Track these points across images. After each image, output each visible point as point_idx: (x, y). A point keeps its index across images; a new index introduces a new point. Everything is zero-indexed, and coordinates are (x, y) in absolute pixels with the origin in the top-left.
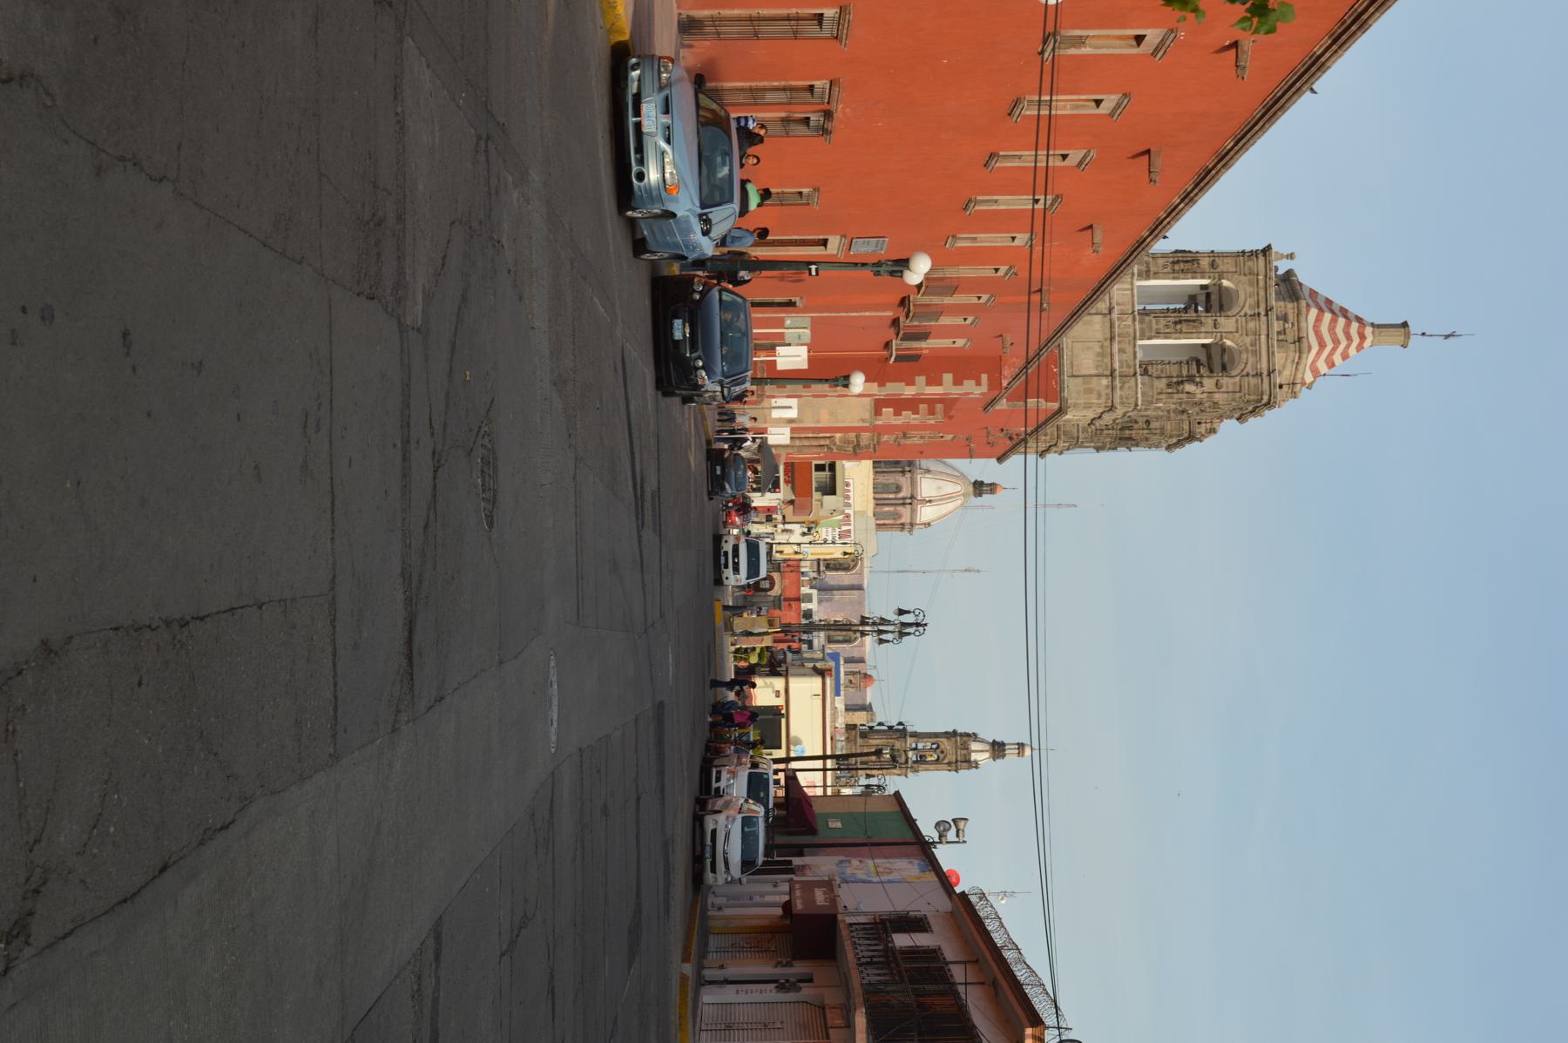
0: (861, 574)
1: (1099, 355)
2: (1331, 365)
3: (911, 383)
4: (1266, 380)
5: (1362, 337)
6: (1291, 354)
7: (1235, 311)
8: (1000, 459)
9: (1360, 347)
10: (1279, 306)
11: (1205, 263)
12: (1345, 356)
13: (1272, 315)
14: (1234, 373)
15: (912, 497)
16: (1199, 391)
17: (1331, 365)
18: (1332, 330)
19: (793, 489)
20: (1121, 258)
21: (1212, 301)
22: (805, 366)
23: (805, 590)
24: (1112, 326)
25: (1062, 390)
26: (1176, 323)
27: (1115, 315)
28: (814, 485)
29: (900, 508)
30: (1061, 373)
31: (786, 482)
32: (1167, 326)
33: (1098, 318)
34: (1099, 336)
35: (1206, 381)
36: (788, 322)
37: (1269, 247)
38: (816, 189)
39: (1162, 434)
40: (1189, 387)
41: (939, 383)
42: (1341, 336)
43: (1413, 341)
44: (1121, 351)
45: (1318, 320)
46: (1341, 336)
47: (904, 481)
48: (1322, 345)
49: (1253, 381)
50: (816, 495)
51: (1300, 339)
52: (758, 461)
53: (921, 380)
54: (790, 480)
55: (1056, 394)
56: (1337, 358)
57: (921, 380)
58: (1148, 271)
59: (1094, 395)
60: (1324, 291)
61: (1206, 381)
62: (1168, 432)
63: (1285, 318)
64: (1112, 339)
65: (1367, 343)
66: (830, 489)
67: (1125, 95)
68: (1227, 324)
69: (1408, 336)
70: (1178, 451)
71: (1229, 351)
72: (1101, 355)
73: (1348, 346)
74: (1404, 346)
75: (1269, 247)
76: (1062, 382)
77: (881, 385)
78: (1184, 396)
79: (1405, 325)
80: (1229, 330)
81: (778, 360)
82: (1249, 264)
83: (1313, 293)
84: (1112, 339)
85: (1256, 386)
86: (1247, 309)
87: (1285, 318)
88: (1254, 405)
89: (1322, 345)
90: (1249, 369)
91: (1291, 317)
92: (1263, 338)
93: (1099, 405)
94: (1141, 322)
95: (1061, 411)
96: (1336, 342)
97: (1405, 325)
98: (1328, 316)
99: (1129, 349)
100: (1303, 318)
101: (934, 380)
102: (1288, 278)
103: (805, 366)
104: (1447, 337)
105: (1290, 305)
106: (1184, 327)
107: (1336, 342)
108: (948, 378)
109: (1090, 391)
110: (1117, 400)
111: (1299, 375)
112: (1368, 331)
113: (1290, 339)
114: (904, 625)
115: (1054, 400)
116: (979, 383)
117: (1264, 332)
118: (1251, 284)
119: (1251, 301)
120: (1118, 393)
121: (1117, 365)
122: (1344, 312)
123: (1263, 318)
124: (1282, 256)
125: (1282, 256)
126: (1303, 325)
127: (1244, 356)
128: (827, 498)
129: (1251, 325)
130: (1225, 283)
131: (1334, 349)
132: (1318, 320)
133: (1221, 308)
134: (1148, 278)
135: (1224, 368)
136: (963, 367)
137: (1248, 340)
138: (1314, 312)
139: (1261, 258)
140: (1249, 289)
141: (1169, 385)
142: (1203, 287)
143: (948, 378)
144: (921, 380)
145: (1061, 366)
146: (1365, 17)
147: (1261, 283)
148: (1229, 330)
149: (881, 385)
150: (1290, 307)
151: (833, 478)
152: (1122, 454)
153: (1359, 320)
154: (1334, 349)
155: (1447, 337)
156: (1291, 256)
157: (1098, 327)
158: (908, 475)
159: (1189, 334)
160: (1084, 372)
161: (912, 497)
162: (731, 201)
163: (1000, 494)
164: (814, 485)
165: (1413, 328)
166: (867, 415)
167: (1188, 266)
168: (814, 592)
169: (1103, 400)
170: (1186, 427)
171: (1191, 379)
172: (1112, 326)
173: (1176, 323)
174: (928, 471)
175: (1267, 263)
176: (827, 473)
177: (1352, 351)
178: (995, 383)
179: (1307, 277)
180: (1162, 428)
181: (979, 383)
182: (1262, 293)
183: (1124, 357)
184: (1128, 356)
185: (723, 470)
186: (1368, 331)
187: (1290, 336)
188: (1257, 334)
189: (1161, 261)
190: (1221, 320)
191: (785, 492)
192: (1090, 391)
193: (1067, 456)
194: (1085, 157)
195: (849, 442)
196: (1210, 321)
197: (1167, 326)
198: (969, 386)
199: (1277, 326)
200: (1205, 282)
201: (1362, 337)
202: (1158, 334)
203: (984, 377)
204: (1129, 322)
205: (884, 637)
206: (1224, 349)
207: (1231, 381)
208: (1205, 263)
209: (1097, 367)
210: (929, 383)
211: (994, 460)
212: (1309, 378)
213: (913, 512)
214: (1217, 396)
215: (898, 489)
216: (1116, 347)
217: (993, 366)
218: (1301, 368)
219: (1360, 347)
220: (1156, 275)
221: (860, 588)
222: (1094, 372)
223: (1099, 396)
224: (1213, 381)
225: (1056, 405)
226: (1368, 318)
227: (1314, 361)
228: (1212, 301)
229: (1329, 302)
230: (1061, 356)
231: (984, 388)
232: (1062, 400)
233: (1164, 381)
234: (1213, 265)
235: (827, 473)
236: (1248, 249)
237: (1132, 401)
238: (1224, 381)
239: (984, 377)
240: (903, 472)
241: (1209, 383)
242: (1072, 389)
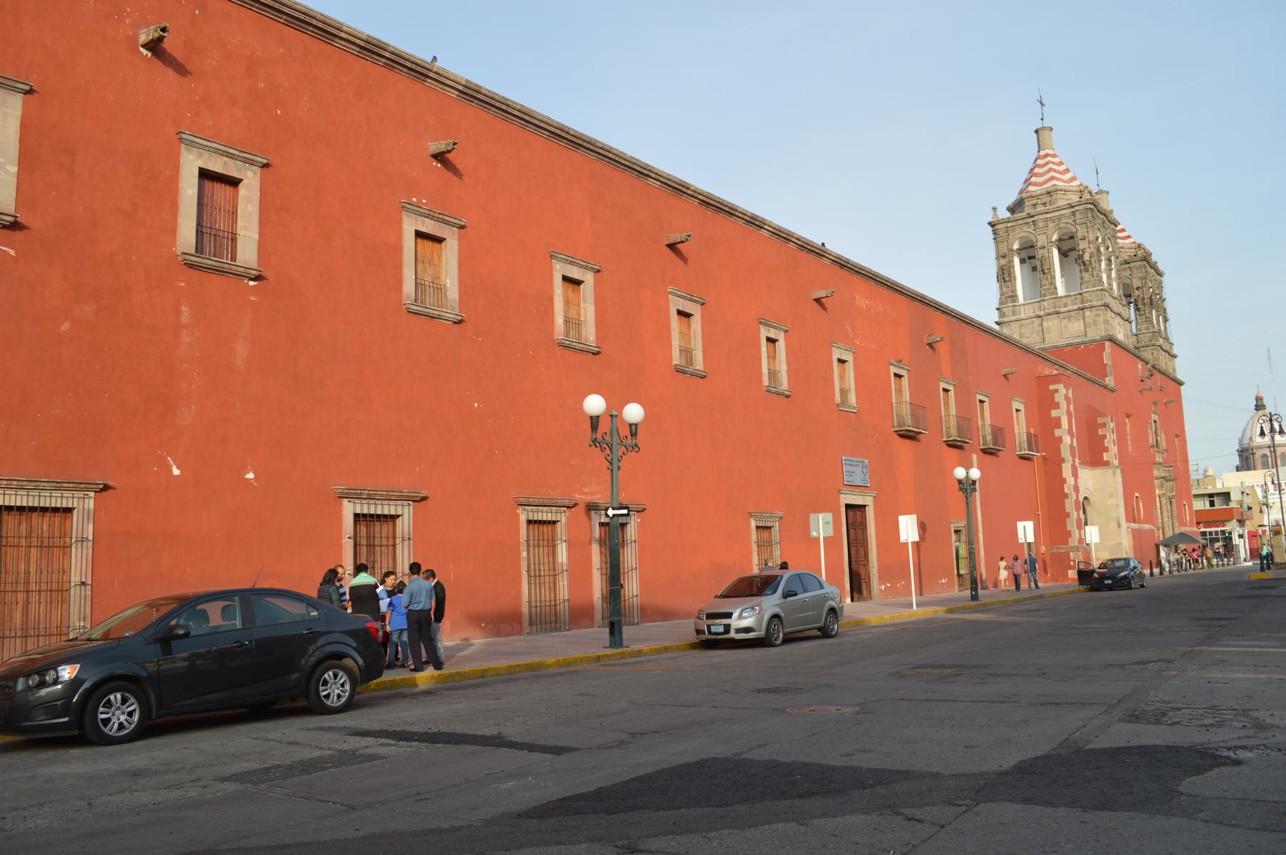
3: (1060, 439)
5: (1047, 155)
7: (1032, 237)
8: (1181, 384)
9: (1054, 156)
10: (1028, 210)
12: (1061, 163)
13: (1033, 211)
20: (872, 282)
27: (1041, 313)
30: (1083, 343)
33: (1045, 324)
34: (1056, 321)
35: (1081, 247)
40: (1086, 257)
41: (1059, 419)
42: (1046, 168)
44: (1066, 305)
45: (1035, 184)
46: (1046, 168)
47: (1259, 453)
48: (1053, 178)
49: (1078, 216)
50: (1233, 505)
51: (1048, 193)
55: (1099, 345)
56: (1061, 168)
57: (1057, 432)
60: (1020, 186)
61: (1081, 247)
63: (1035, 205)
65: (1051, 152)
66: (1226, 496)
68: (1041, 240)
70: (1161, 267)
72: (1069, 318)
77: (1063, 461)
79: (1037, 132)
83: (1021, 192)
87: (1035, 205)
89: (1053, 178)
90: (1070, 221)
95: (1112, 340)
96: (1050, 170)
97: (1037, 132)
98: (1033, 179)
99: (1064, 300)
102: (1012, 210)
103: (901, 518)
104: (1042, 104)
106: (1046, 267)
108: (1054, 413)
109: (1095, 323)
110: (1100, 303)
112: (1042, 153)
114: (1272, 430)
115: (1103, 346)
116: (1057, 391)
120: (1095, 303)
122: (1032, 170)
124: (995, 215)
125: (995, 215)
128: (1233, 497)
129: (1041, 225)
130: (1016, 246)
132: (1035, 184)
133: (1032, 247)
134: (1016, 296)
136: (1043, 404)
137: (1051, 225)
138: (1031, 188)
142: (1022, 261)
143: (1054, 413)
144: (1057, 432)
145: (1079, 344)
146: (362, 44)
149: (1063, 461)
151: (1219, 494)
154: (1059, 172)
155: (1042, 104)
156: (995, 209)
157: (1050, 324)
160: (1082, 327)
163: (1262, 394)
165: (1039, 125)
166: (1110, 471)
171: (1081, 257)
174: (1251, 439)
175: (1000, 222)
177: (1056, 160)
178: (1056, 379)
179: (1012, 198)
181: (1057, 391)
184: (1069, 300)
185: (1108, 578)
187: (1047, 199)
190: (1039, 244)
191: (1232, 527)
192: (1095, 323)
194: (675, 295)
196: (1041, 252)
198: (1059, 397)
199: (1040, 208)
200: (1016, 260)
201: (1047, 155)
202: (1053, 284)
203: (1052, 387)
206: (1060, 240)
208: (1003, 262)
210: (1059, 426)
212: (1076, 183)
215: (1265, 456)
216: (1063, 309)
217: (1044, 381)
219: (1054, 156)
220: (1014, 291)
225: (1107, 344)
226: (1035, 155)
228: (1029, 254)
229: (1026, 181)
230: (1072, 345)
231: (1061, 387)
232: (1103, 340)
233: (1084, 274)
234: (1004, 257)
238: (1080, 235)
239: (1052, 387)
241: (1083, 245)
242: (1094, 334)
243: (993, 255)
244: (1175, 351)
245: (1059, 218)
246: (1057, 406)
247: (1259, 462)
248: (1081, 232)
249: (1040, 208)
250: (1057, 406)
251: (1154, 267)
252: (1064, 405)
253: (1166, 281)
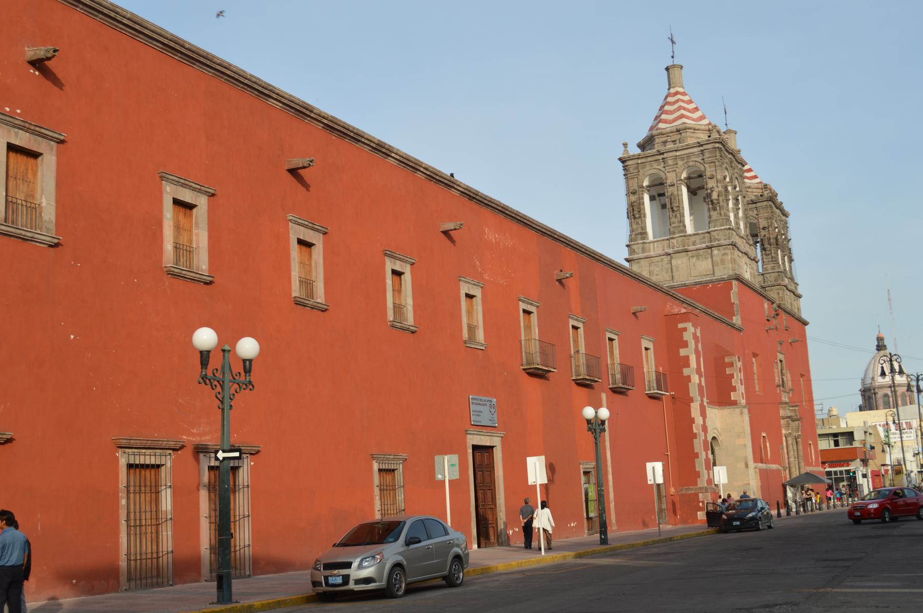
1: (698, 258)
2: (696, 109)
3: (688, 378)
4: (705, 147)
5: (677, 93)
6: (688, 134)
8: (805, 323)
9: (684, 94)
10: (658, 147)
11: (633, 198)
12: (690, 102)
13: (662, 149)
14: (703, 169)
15: (890, 387)
17: (696, 109)
18: (672, 112)
19: (852, 460)
20: (502, 216)
21: (659, 191)
24: (678, 252)
25: (722, 280)
26: (673, 211)
27: (671, 251)
28: (849, 446)
29: (898, 394)
30: (711, 281)
31: (848, 465)
32: (676, 216)
33: (674, 262)
34: (685, 259)
35: (710, 186)
36: (440, 477)
37: (620, 159)
38: (373, 457)
39: (771, 218)
40: (715, 196)
41: (687, 357)
43: (677, 62)
45: (665, 122)
47: (880, 393)
48: (682, 116)
49: (707, 155)
50: (856, 444)
51: (678, 131)
52: (802, 488)
53: (686, 372)
54: (847, 462)
55: (726, 284)
58: (641, 233)
59: (725, 257)
60: (650, 122)
61: (710, 186)
62: (770, 215)
63: (665, 142)
64: (686, 251)
65: (681, 90)
66: (850, 435)
68: (671, 178)
69: (674, 66)
70: (786, 207)
71: (682, 169)
72: (698, 256)
73: (683, 101)
74: (681, 67)
75: (620, 159)
77: (691, 400)
78: (721, 198)
79: (667, 69)
80: (677, 177)
81: (539, 482)
82: (631, 170)
83: (651, 129)
84: (686, 251)
85: (710, 152)
86: (661, 167)
87: (665, 142)
89: (682, 116)
90: (699, 159)
91: (664, 139)
92: (678, 153)
93: (732, 254)
95: (739, 279)
96: (680, 108)
97: (667, 69)
99: (693, 239)
100: (664, 131)
101: (686, 362)
102: (642, 146)
104: (673, 42)
105: (657, 141)
106: (674, 205)
107: (680, 108)
109: (723, 261)
110: (727, 242)
111: (703, 127)
112: (672, 91)
113: (679, 136)
114: (892, 370)
116: (685, 329)
117: (674, 154)
118: (644, 167)
119: (655, 165)
120: (723, 242)
121: (704, 245)
123: (665, 155)
124: (626, 151)
125: (626, 151)
126: (668, 130)
127: (691, 164)
128: (856, 437)
129: (670, 162)
131: (685, 109)
132: (665, 122)
135: (700, 176)
137: (680, 163)
138: (661, 125)
139: (628, 163)
140: (648, 167)
141: (715, 209)
142: (652, 198)
143: (683, 352)
144: (686, 372)
145: (707, 282)
147: (643, 160)
148: (677, 177)
149: (691, 400)
150: (658, 140)
151: (843, 434)
152: (793, 245)
153: (666, 97)
155: (673, 42)
156: (625, 145)
157: (679, 261)
158: (877, 390)
159: (680, 201)
160: (711, 267)
164: (849, 446)
166: (738, 411)
167: (636, 209)
169: (728, 251)
171: (709, 195)
172: (678, 252)
173: (673, 211)
176: (840, 438)
177: (686, 98)
178: (684, 318)
180: (767, 218)
181: (685, 329)
182: (649, 159)
183: (698, 241)
185: (737, 520)
186: (672, 91)
187: (676, 137)
188: (676, 157)
189: (635, 226)
190: (669, 182)
191: (856, 466)
192: (723, 261)
196: (670, 189)
197: (676, 216)
198: (688, 336)
200: (646, 197)
201: (677, 93)
203: (680, 326)
204: (674, 241)
206: (689, 178)
207: (708, 170)
208: (633, 198)
209: (706, 258)
210: (688, 366)
212: (705, 122)
213: (899, 385)
215: (886, 395)
216: (691, 248)
218: (697, 127)
222: (710, 260)
223: (725, 254)
225: (735, 283)
226: (665, 93)
227: (693, 120)
229: (657, 118)
230: (700, 283)
231: (689, 325)
233: (712, 213)
234: (634, 193)
235: (840, 438)
236: (623, 172)
237: (727, 232)
238: (708, 174)
239: (680, 326)
240: (875, 394)
242: (722, 273)
243: (623, 190)
244: (800, 291)
245: (688, 156)
246: (685, 345)
247: (880, 402)
248: (709, 171)
249: (670, 146)
250: (685, 345)
251: (779, 207)
252: (692, 344)
253: (791, 221)
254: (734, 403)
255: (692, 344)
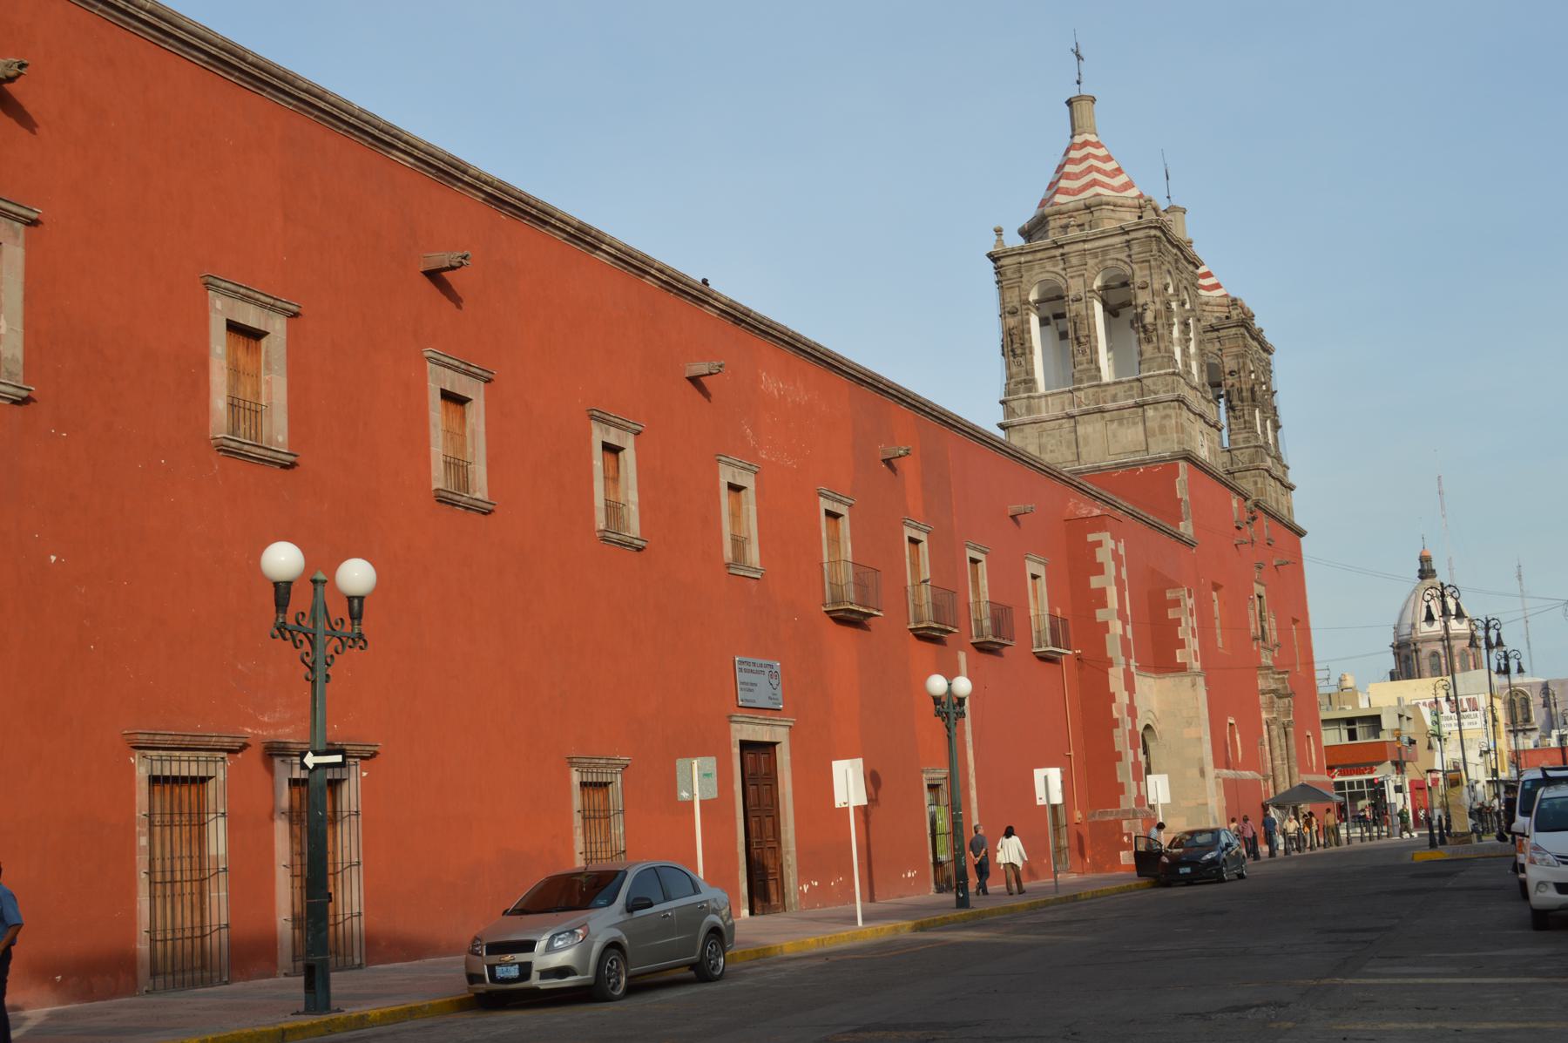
0: (1529, 685)
2: (1119, 171)
3: (1105, 627)
4: (1133, 235)
5: (1086, 144)
6: (1105, 213)
8: (1300, 533)
9: (1098, 145)
10: (1054, 235)
12: (1108, 159)
14: (1129, 272)
15: (1442, 640)
16: (1152, 307)
17: (1119, 171)
18: (1077, 176)
19: (1379, 763)
20: (789, 352)
21: (1055, 309)
22: (860, 761)
23: (1554, 742)
25: (1162, 460)
26: (1079, 343)
27: (1075, 411)
29: (1455, 651)
31: (1371, 772)
32: (1084, 352)
34: (1099, 426)
35: (1140, 301)
36: (685, 795)
37: (990, 255)
39: (1243, 356)
40: (1149, 318)
42: (1084, 165)
45: (1067, 192)
46: (1084, 165)
47: (1426, 650)
48: (1094, 183)
49: (1136, 248)
50: (1385, 737)
51: (1088, 207)
53: (1101, 615)
55: (1168, 466)
58: (1025, 382)
60: (1041, 192)
61: (1140, 301)
62: (1241, 350)
64: (1102, 411)
65: (1092, 138)
66: (1374, 721)
67: (207, 286)
68: (1075, 287)
69: (1080, 98)
70: (1269, 337)
71: (1096, 274)
72: (1121, 420)
74: (1093, 100)
75: (990, 255)
76: (1154, 461)
77: (1110, 663)
78: (1159, 322)
79: (1069, 103)
82: (1009, 274)
83: (1042, 204)
84: (1102, 411)
86: (1058, 269)
87: (1065, 227)
88: (1161, 237)
89: (1094, 183)
90: (1123, 256)
91: (1064, 222)
92: (1087, 246)
93: (1179, 416)
94: (1081, 381)
95: (1189, 458)
96: (1091, 169)
97: (1069, 103)
98: (1063, 183)
99: (1112, 390)
100: (1064, 208)
101: (1100, 598)
103: (860, 761)
104: (1079, 57)
105: (1052, 224)
106: (1082, 333)
107: (1091, 169)
108: (1095, 582)
110: (1170, 396)
111: (1130, 202)
112: (1078, 140)
113: (1088, 217)
114: (1445, 612)
116: (1099, 544)
117: (1081, 246)
118: (1031, 269)
119: (1049, 266)
120: (1162, 396)
121: (1131, 402)
122: (1061, 167)
123: (1067, 249)
124: (1000, 241)
125: (1000, 241)
126: (1071, 206)
127: (1109, 263)
128: (1385, 725)
129: (1074, 261)
130: (1033, 296)
131: (1099, 170)
132: (1067, 192)
133: (1060, 297)
137: (1091, 262)
140: (1037, 269)
141: (1149, 341)
142: (1044, 322)
143: (1095, 582)
144: (1101, 615)
145: (1136, 464)
147: (1029, 258)
149: (1110, 663)
151: (1363, 719)
154: (1099, 170)
155: (1079, 57)
156: (999, 231)
157: (1090, 429)
158: (1419, 646)
160: (1142, 437)
161: (1442, 640)
162: (1542, 800)
163: (1430, 552)
165: (1073, 93)
166: (1187, 680)
167: (1016, 339)
168: (1555, 733)
170: (1233, 331)
171: (1140, 317)
173: (1079, 343)
177: (1101, 152)
178: (1098, 524)
179: (1028, 214)
180: (1237, 356)
181: (1099, 544)
182: (1039, 255)
183: (1121, 394)
184: (1119, 390)
185: (1185, 864)
186: (1078, 140)
187: (1084, 218)
190: (1072, 294)
191: (1384, 773)
192: (1162, 429)
193: (1288, 458)
195: (1272, 702)
196: (1074, 307)
198: (1103, 555)
200: (1034, 320)
201: (1086, 144)
202: (1094, 361)
203: (1091, 537)
204: (1081, 394)
205: (1494, 640)
207: (1138, 273)
208: (1012, 321)
209: (1135, 423)
210: (1104, 605)
211: (1302, 540)
212: (1133, 192)
213: (1457, 637)
214: (1156, 286)
215: (1435, 654)
216: (1110, 405)
217: (1079, 527)
218: (1120, 202)
220: (1030, 372)
221: (1545, 688)
223: (1167, 416)
224: (1140, 293)
225: (1182, 465)
226: (1067, 142)
227: (1113, 189)
228: (1055, 309)
229: (1051, 185)
230: (1124, 465)
231: (1106, 537)
233: (1145, 347)
234: (1013, 313)
235: (1357, 726)
237: (1169, 379)
238: (1138, 280)
239: (1091, 537)
242: (1162, 448)
243: (995, 309)
244: (1292, 478)
245: (1105, 250)
246: (1099, 569)
247: (1426, 665)
248: (1140, 276)
249: (1074, 233)
250: (1099, 569)
251: (1257, 337)
252: (1110, 568)
253: (1278, 361)
254: (1182, 668)
255: (1110, 568)
